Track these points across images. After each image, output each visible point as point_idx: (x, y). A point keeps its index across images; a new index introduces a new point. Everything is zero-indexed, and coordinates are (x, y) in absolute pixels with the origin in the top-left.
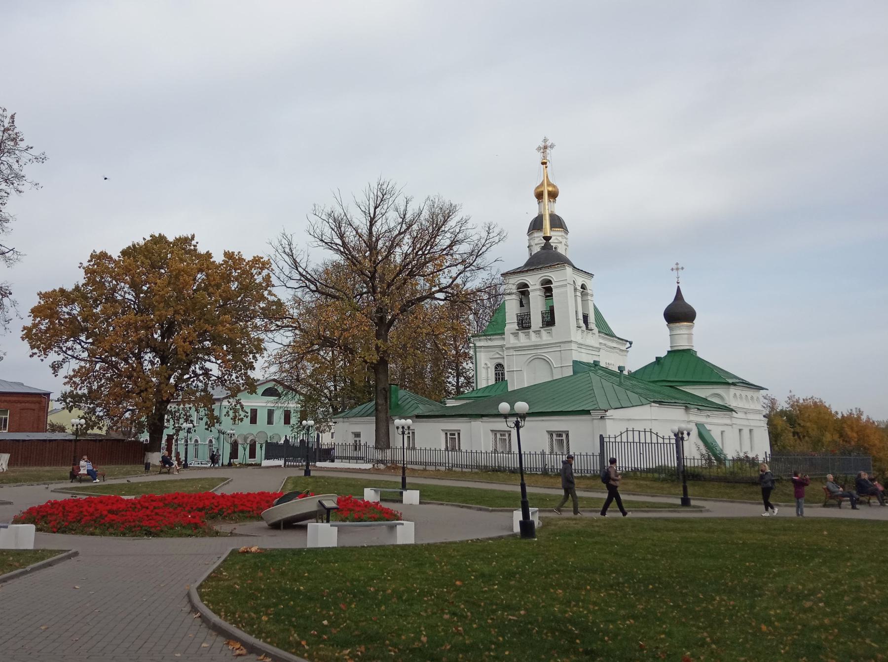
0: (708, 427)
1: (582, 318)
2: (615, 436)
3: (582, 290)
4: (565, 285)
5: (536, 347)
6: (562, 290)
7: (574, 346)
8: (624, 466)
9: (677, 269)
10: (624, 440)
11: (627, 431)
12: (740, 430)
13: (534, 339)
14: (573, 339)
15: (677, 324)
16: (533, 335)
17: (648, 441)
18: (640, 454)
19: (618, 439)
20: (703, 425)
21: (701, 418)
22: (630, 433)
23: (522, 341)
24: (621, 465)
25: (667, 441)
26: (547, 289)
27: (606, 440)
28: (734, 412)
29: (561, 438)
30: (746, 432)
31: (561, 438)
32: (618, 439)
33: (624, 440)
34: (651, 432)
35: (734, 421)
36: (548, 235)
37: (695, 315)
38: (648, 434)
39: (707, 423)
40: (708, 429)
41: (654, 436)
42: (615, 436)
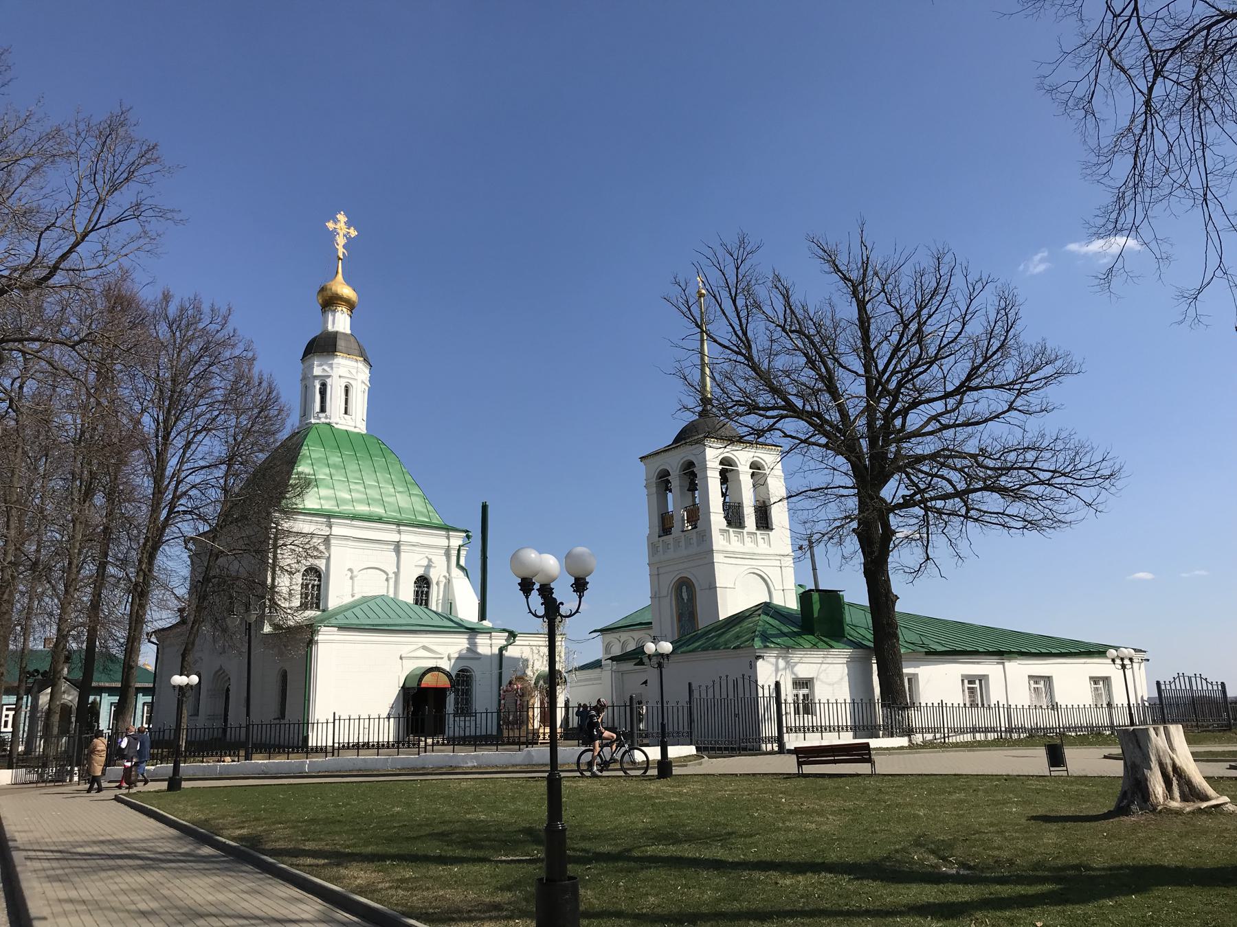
25: (1215, 688)
34: (1201, 678)
38: (1198, 679)
41: (1204, 682)
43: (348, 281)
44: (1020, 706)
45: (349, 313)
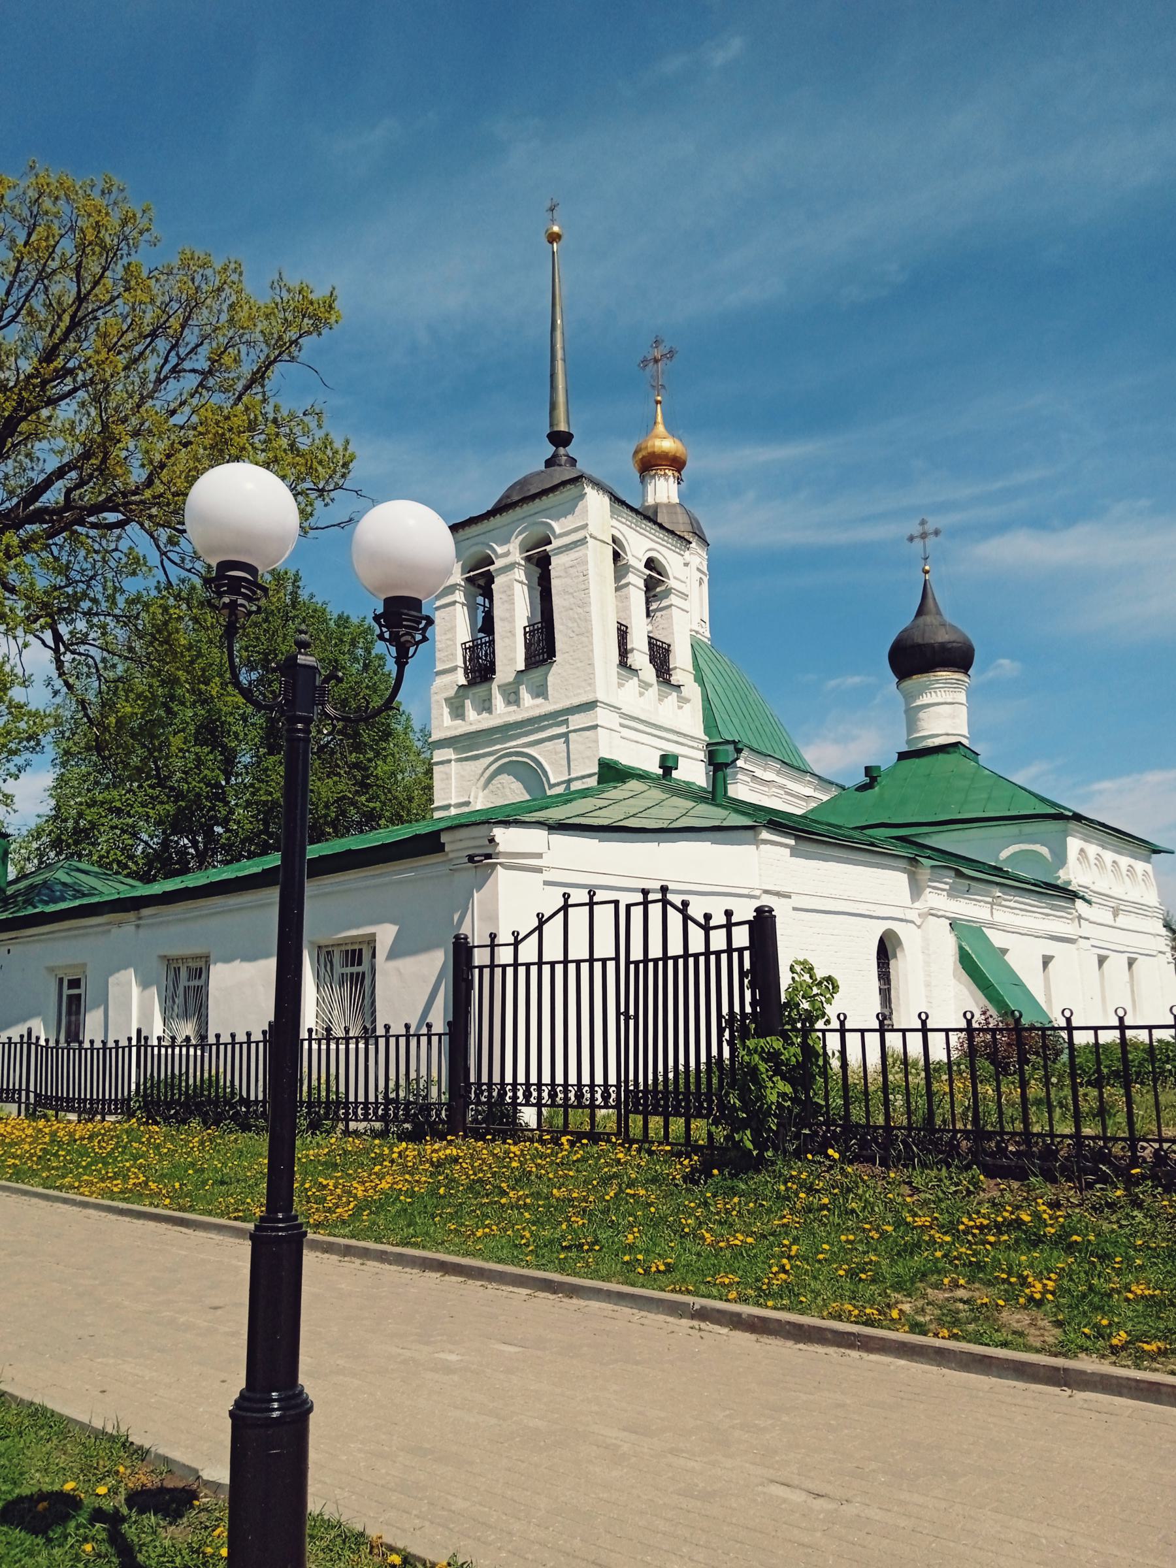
0: (997, 939)
1: (646, 648)
2: (515, 934)
3: (648, 572)
4: (583, 541)
5: (505, 731)
6: (572, 555)
7: (602, 716)
8: (546, 1079)
9: (924, 536)
10: (553, 952)
11: (565, 908)
12: (1102, 960)
13: (502, 712)
14: (600, 696)
15: (932, 676)
16: (498, 701)
17: (675, 948)
18: (618, 1014)
19: (528, 953)
20: (980, 928)
21: (972, 909)
22: (579, 916)
23: (472, 718)
24: (534, 1079)
26: (540, 566)
27: (480, 957)
28: (1079, 903)
29: (355, 969)
30: (1117, 963)
31: (355, 969)
32: (528, 953)
33: (553, 952)
35: (1086, 929)
36: (562, 429)
37: (973, 650)
38: (655, 910)
39: (992, 926)
40: (997, 945)
41: (675, 918)
42: (515, 934)
43: (672, 431)
44: (398, 1029)
45: (676, 474)
